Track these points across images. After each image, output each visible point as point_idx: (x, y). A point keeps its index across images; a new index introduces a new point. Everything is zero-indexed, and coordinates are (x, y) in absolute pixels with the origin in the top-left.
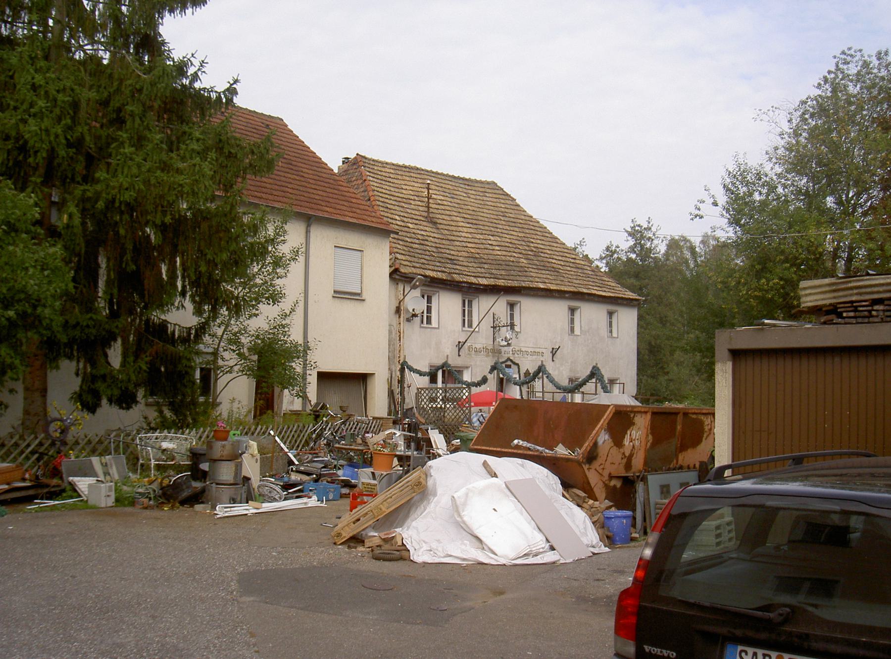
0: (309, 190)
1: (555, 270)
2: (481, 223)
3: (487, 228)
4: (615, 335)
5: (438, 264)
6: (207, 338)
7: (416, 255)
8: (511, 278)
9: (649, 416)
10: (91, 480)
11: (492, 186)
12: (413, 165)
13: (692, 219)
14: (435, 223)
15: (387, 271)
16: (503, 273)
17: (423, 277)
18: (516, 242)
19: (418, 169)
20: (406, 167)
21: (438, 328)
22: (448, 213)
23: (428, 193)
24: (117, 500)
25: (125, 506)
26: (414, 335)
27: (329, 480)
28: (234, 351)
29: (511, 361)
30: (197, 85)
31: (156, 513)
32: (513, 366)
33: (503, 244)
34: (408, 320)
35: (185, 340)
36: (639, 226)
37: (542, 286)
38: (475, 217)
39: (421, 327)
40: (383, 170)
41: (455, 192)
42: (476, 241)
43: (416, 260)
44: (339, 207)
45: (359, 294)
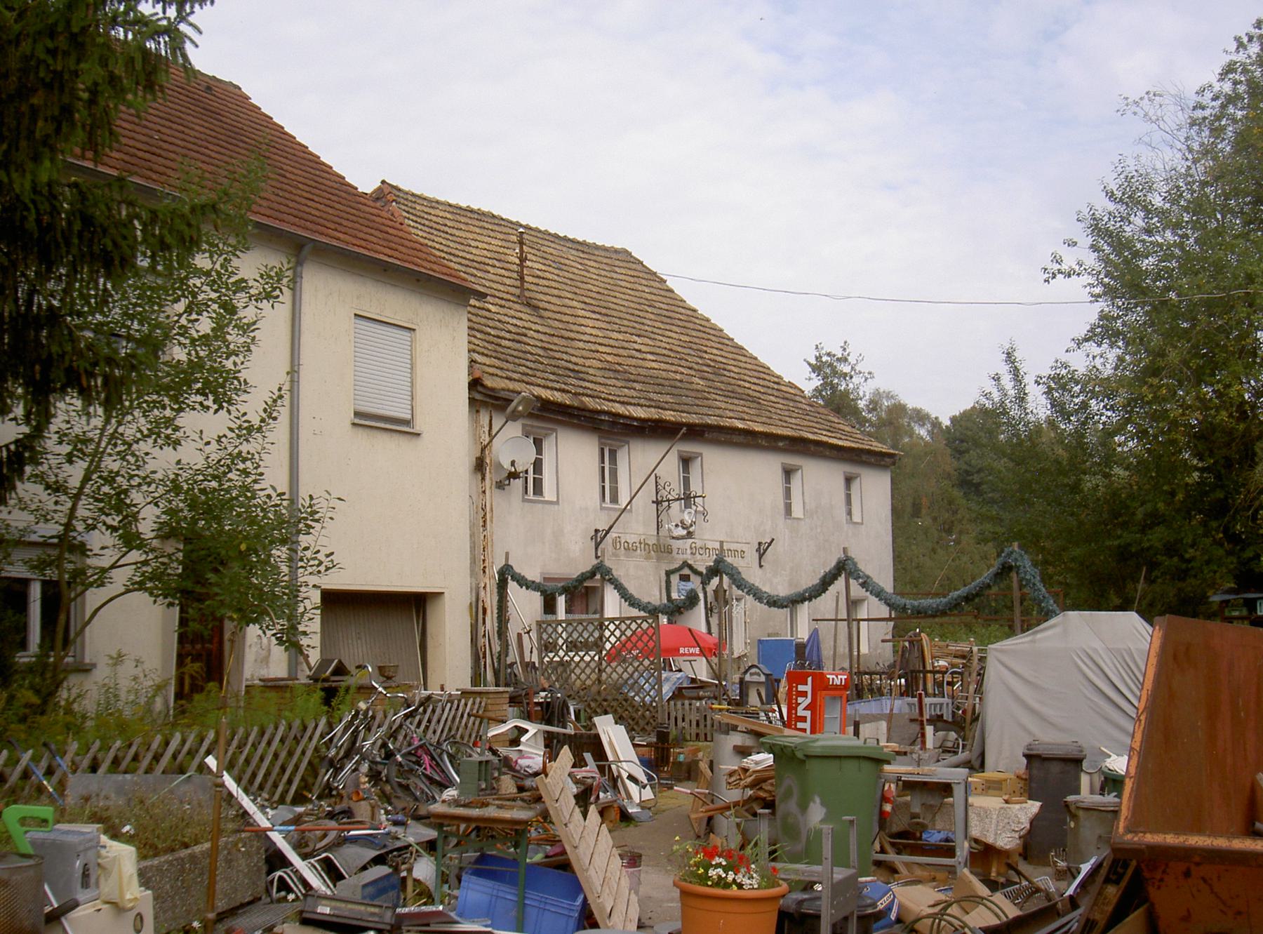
0: (297, 198)
1: (754, 400)
3: (626, 323)
4: (856, 518)
5: (552, 377)
6: (27, 489)
7: (510, 359)
11: (624, 256)
12: (485, 209)
13: (1047, 281)
14: (536, 308)
15: (464, 380)
16: (669, 398)
18: (679, 349)
19: (494, 216)
20: (472, 211)
21: (557, 503)
22: (556, 292)
23: (522, 251)
26: (511, 513)
28: (114, 529)
29: (690, 567)
32: (693, 577)
33: (658, 350)
34: (500, 485)
36: (828, 354)
37: (740, 425)
39: (524, 500)
40: (432, 211)
42: (612, 342)
43: (511, 367)
45: (407, 423)
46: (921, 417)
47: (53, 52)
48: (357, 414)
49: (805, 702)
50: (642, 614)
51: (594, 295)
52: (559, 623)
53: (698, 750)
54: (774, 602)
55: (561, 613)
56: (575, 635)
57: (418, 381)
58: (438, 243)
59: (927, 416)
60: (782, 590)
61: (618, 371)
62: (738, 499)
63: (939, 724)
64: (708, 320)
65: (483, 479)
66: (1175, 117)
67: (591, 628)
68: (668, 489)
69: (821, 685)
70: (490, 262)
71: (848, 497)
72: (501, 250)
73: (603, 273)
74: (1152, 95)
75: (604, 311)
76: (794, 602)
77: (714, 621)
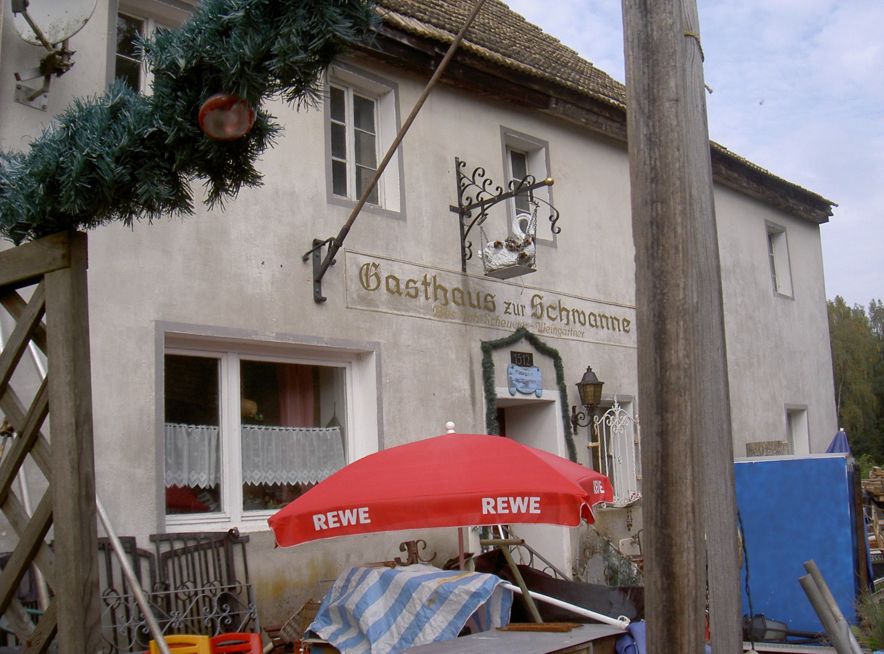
29: (532, 340)
32: (537, 358)
68: (479, 181)
77: (582, 442)
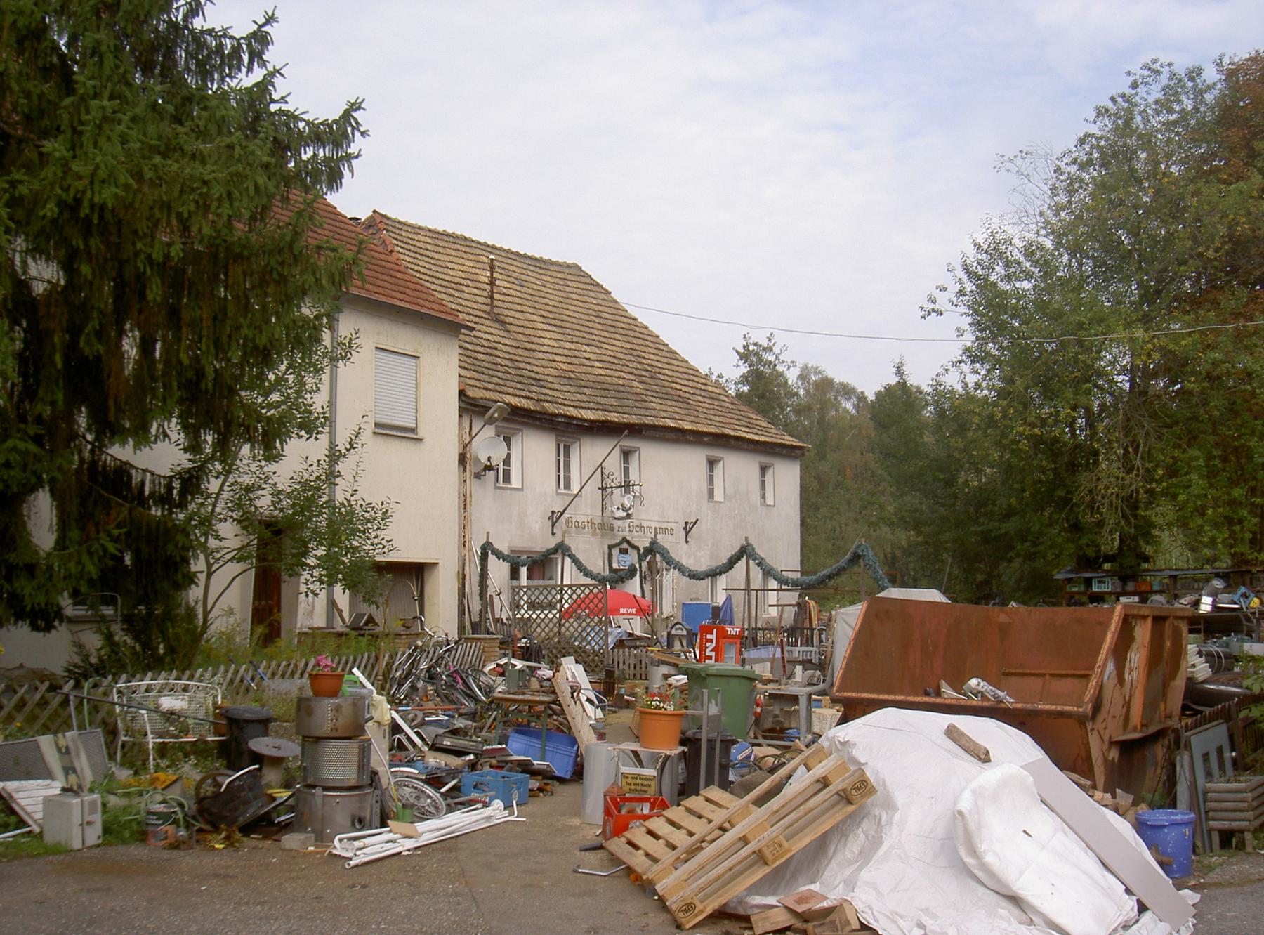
1: (685, 401)
2: (567, 325)
3: (577, 333)
4: (769, 501)
5: (519, 386)
7: (486, 371)
8: (627, 410)
9: (1149, 621)
10: (53, 788)
12: (458, 232)
13: (923, 317)
14: (503, 323)
16: (613, 402)
17: (506, 408)
19: (466, 239)
20: (447, 235)
21: (522, 489)
22: (519, 307)
24: (107, 830)
25: (125, 842)
27: (494, 762)
29: (628, 542)
30: (198, 23)
31: (189, 860)
33: (605, 358)
34: (477, 476)
35: (164, 499)
36: (755, 344)
37: (672, 424)
38: (557, 316)
39: (496, 488)
41: (524, 277)
42: (566, 352)
43: (486, 378)
44: (378, 282)
45: (412, 430)
46: (847, 391)
47: (282, 263)
48: (377, 425)
49: (711, 646)
50: (594, 582)
51: (551, 309)
52: (521, 588)
53: (635, 686)
54: (694, 576)
55: (524, 580)
56: (541, 597)
57: (422, 399)
58: (417, 267)
59: (853, 391)
60: (703, 566)
61: (570, 378)
62: (667, 486)
63: (808, 665)
64: (646, 328)
65: (465, 470)
66: (1042, 176)
67: (554, 592)
69: (722, 635)
70: (465, 282)
71: (763, 484)
72: (474, 270)
73: (557, 287)
74: (1025, 154)
75: (559, 323)
76: (714, 574)
